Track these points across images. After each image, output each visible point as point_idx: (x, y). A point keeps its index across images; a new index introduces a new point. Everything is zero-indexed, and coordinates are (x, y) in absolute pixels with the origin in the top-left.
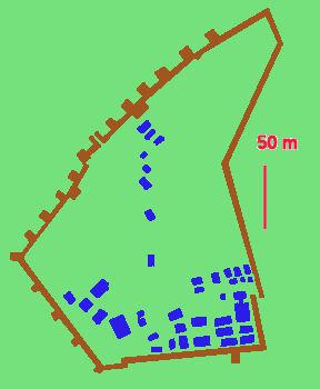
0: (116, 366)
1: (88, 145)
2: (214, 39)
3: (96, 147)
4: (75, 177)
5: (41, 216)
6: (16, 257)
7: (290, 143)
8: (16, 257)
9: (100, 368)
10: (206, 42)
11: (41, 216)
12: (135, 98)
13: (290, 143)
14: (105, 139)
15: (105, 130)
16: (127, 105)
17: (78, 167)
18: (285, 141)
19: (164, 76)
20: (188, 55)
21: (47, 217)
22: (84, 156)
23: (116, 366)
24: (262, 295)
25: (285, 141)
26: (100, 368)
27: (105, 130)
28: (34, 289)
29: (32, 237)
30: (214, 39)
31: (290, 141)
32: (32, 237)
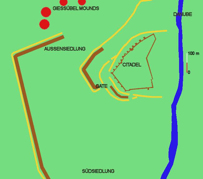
0: (128, 90)
1: (124, 55)
2: (145, 38)
3: (125, 55)
4: (133, 47)
5: (139, 40)
6: (112, 73)
7: (198, 53)
8: (112, 73)
9: (126, 91)
10: (119, 64)
11: (139, 40)
12: (131, 48)
13: (198, 53)
14: (127, 54)
15: (126, 53)
16: (130, 49)
17: (122, 59)
18: (196, 53)
19: (136, 44)
20: (140, 41)
21: (136, 44)
22: (123, 57)
23: (128, 90)
24: (151, 79)
25: (196, 53)
26: (126, 91)
27: (126, 53)
28: (115, 78)
29: (114, 70)
30: (145, 38)
31: (198, 53)
32: (114, 70)
